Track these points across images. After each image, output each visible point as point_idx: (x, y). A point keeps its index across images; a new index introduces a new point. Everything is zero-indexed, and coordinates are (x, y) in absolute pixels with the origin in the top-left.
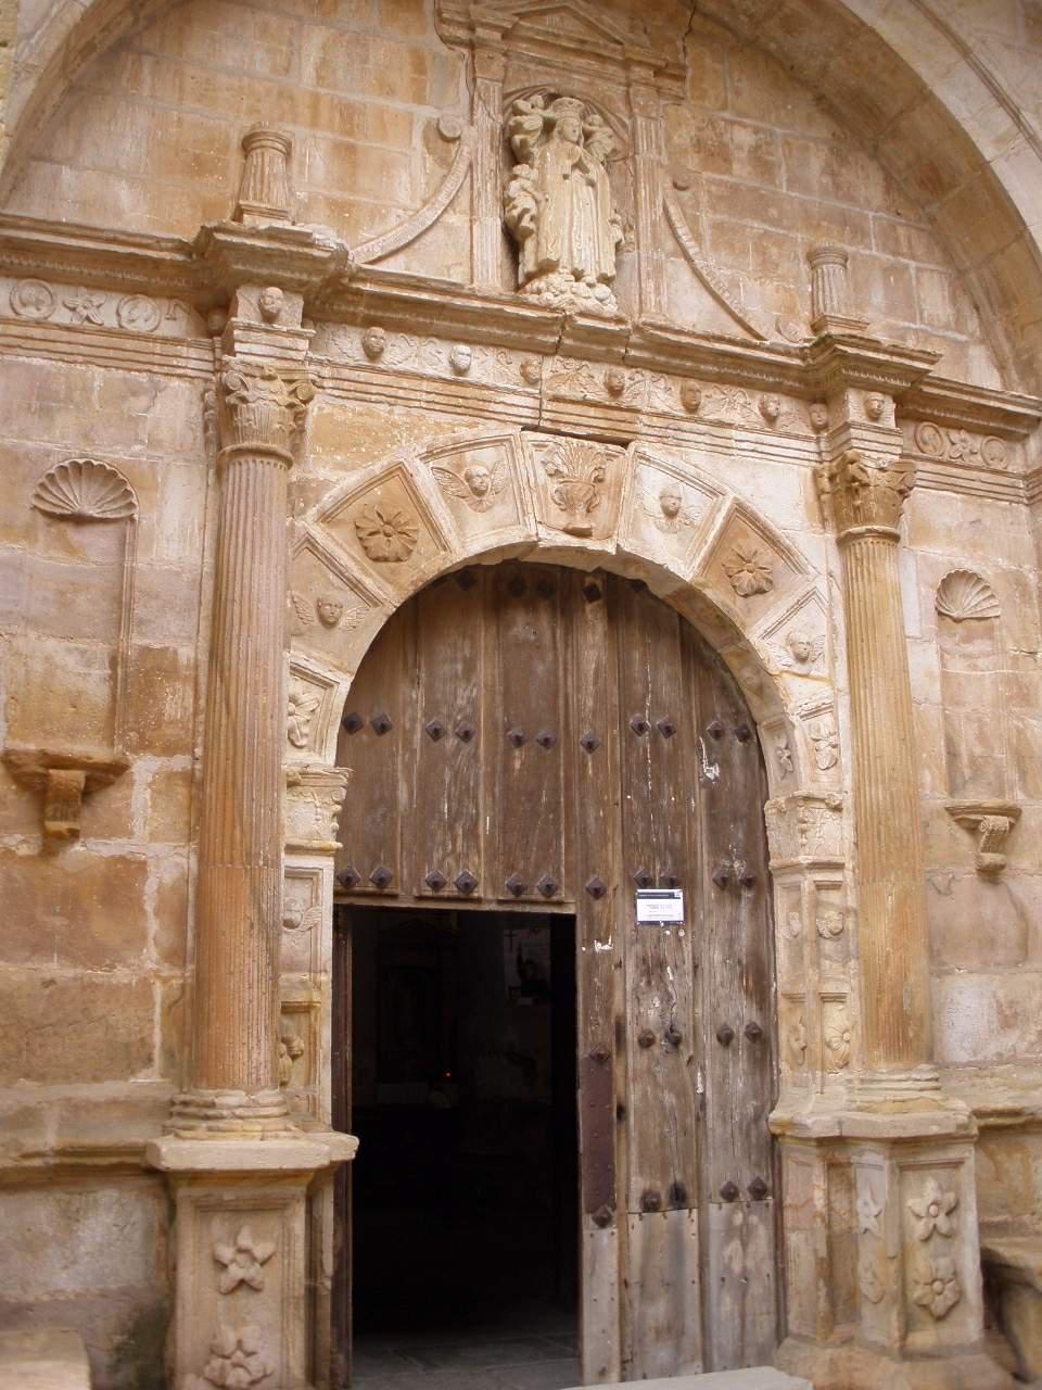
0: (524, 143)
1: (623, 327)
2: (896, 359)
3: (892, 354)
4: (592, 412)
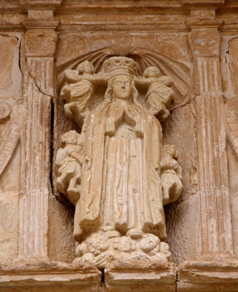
0: (74, 110)
1: (165, 274)
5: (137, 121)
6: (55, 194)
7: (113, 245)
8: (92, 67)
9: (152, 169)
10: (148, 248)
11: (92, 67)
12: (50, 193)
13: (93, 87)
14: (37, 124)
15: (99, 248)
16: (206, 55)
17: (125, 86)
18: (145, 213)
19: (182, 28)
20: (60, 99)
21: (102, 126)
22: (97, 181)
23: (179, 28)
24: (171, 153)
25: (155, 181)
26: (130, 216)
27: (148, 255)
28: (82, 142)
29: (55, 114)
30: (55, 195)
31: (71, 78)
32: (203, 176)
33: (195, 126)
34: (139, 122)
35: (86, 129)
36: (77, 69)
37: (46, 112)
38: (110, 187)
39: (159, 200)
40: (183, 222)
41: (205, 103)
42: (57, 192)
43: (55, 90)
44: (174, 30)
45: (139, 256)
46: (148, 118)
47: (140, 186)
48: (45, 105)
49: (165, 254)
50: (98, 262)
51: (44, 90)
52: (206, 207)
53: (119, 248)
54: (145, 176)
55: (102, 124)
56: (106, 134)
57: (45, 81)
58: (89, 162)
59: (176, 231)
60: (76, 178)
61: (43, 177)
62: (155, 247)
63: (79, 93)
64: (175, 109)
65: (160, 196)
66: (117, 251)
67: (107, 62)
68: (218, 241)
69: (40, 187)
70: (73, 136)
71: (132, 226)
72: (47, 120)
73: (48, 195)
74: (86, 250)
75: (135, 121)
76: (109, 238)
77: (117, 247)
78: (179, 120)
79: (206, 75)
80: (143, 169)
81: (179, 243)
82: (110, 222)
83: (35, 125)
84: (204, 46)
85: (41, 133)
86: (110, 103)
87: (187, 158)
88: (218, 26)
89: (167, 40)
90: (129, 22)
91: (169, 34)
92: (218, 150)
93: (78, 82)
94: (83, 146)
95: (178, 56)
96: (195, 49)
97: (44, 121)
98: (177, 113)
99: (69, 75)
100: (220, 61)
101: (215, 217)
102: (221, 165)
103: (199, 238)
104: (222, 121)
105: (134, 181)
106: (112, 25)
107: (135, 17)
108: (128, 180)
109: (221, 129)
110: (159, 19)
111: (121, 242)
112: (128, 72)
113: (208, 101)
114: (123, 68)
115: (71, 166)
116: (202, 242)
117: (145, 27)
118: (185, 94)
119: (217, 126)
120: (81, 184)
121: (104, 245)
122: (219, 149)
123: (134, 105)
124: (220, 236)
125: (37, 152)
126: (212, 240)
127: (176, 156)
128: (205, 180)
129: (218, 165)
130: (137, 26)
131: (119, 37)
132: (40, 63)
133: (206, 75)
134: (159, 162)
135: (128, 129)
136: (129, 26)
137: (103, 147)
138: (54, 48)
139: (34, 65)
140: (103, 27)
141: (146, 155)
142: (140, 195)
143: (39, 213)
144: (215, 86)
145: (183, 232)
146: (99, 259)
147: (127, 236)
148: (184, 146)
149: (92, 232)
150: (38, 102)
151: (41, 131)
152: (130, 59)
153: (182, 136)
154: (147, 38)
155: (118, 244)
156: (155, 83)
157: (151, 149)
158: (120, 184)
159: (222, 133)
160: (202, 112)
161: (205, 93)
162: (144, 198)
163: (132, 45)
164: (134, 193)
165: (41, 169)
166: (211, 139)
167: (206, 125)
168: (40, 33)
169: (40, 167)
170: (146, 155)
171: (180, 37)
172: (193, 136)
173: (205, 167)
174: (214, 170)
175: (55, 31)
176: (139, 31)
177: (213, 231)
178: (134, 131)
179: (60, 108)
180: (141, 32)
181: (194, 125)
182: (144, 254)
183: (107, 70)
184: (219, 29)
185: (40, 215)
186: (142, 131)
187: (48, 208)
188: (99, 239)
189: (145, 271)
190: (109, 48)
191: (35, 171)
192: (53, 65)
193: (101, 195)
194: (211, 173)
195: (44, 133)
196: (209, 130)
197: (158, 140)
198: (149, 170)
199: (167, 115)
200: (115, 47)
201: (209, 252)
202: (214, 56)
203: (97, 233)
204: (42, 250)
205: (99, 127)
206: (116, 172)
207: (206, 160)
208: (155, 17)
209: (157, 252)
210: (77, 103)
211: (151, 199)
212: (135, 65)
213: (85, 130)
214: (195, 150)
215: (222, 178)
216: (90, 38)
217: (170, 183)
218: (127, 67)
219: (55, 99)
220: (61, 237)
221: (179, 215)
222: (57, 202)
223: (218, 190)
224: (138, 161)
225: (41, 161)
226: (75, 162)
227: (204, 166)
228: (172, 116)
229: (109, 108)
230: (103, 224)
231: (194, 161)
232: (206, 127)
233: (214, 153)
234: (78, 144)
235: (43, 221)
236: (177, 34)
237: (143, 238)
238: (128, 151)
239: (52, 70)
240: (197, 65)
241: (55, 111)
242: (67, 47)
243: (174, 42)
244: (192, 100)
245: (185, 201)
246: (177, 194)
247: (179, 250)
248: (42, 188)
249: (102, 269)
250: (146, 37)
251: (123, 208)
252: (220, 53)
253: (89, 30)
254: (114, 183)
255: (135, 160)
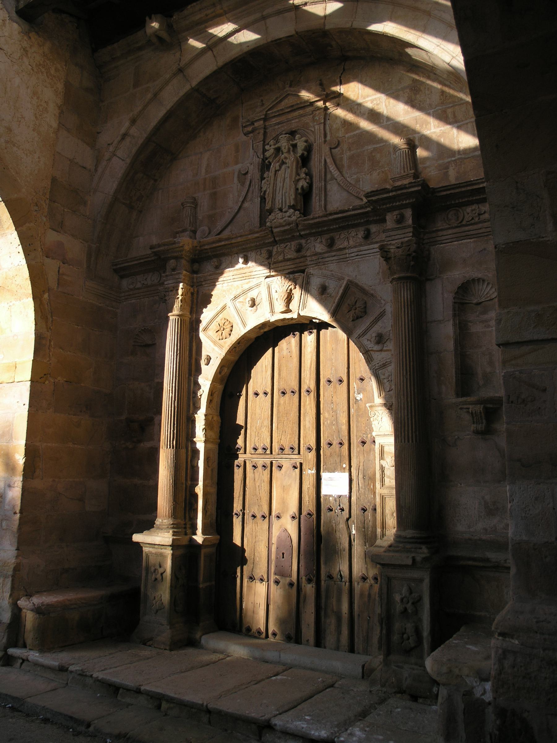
2: (399, 192)
3: (396, 191)
4: (288, 263)
68: (319, 206)
79: (318, 133)
89: (306, 121)
91: (306, 117)
133: (318, 133)
212: (290, 137)
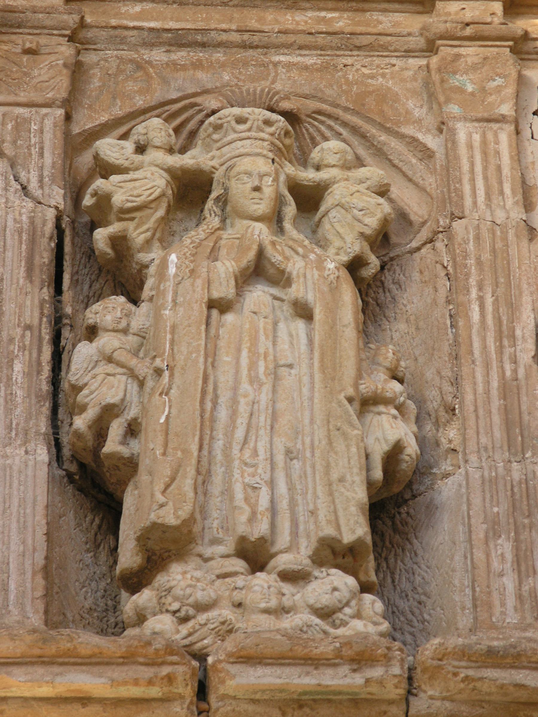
5: (295, 273)
6: (64, 467)
7: (230, 596)
8: (170, 136)
9: (337, 399)
10: (327, 607)
11: (170, 136)
12: (53, 463)
13: (174, 186)
14: (18, 279)
15: (191, 600)
16: (480, 115)
17: (261, 184)
18: (319, 512)
19: (412, 46)
20: (80, 223)
21: (199, 282)
22: (185, 425)
23: (406, 47)
24: (388, 364)
25: (346, 428)
26: (279, 518)
27: (328, 624)
28: (141, 327)
29: (67, 258)
30: (64, 470)
31: (113, 160)
32: (475, 427)
33: (449, 298)
34: (301, 275)
35: (154, 293)
36: (130, 139)
37: (42, 248)
38: (221, 443)
39: (357, 479)
40: (418, 552)
41: (477, 238)
42: (72, 462)
43: (68, 195)
44: (391, 52)
45: (303, 626)
46: (325, 268)
47: (303, 443)
48: (39, 229)
49: (375, 624)
50: (190, 639)
51: (38, 193)
52: (485, 507)
53: (248, 602)
54: (319, 418)
55: (199, 277)
56: (212, 304)
57: (42, 168)
58: (167, 373)
59: (397, 577)
60: (127, 420)
61: (34, 418)
62: (347, 604)
63: (134, 199)
64: (392, 259)
65: (361, 470)
66: (239, 611)
67: (213, 122)
68: (520, 597)
69: (25, 443)
70: (119, 309)
71: (283, 547)
72: (45, 268)
73: (46, 465)
74: (155, 607)
75: (290, 274)
76: (218, 577)
77: (242, 599)
78: (403, 287)
79: (479, 168)
80: (311, 399)
81: (407, 608)
82: (221, 535)
83: (11, 281)
84: (472, 94)
85: (28, 303)
86: (218, 229)
87: (427, 382)
88: (511, 43)
89: (372, 77)
90: (270, 27)
91: (377, 61)
92: (514, 361)
93: (131, 172)
94: (144, 338)
95: (402, 119)
96: (448, 100)
97: (37, 271)
98: (398, 269)
99: (108, 152)
100: (518, 133)
101: (509, 533)
102: (524, 399)
103: (464, 591)
104: (525, 286)
105: (289, 429)
106: (224, 34)
107: (286, 15)
108: (272, 428)
109: (522, 305)
110: (350, 22)
111: (252, 587)
112: (270, 151)
113: (486, 235)
114: (256, 139)
115: (113, 387)
116: (474, 599)
117: (314, 40)
118: (421, 220)
119: (511, 299)
120: (142, 435)
121: (205, 592)
122: (518, 358)
123: (284, 238)
124: (525, 583)
125: (16, 351)
126: (502, 593)
127: (400, 374)
128: (480, 437)
129: (516, 398)
130: (291, 38)
131: (241, 64)
132: (28, 121)
133: (479, 168)
134: (357, 382)
135: (271, 295)
136: (269, 37)
137: (203, 335)
138: (65, 85)
139: (9, 127)
140: (199, 38)
141: (320, 362)
142: (305, 467)
143: (22, 512)
144: (505, 196)
145: (418, 579)
146: (191, 630)
147: (269, 573)
148: (417, 353)
149: (172, 561)
150: (20, 222)
151: (29, 297)
152: (275, 117)
153: (414, 327)
154: (317, 70)
155: (244, 592)
156: (342, 184)
157: (335, 348)
158: (250, 434)
159: (524, 316)
160: (471, 261)
161: (477, 212)
162: (317, 472)
163: (278, 86)
164: (288, 460)
165: (29, 396)
166: (495, 331)
167: (481, 294)
168: (28, 45)
169: (26, 389)
170: (322, 361)
171: (407, 69)
172: (445, 324)
173: (480, 403)
174: (506, 411)
175: (68, 41)
176: (298, 52)
177: (503, 570)
178: (286, 302)
179: (79, 245)
180: (301, 55)
181: (447, 297)
182: (318, 621)
183: (211, 143)
184: (513, 50)
185: (24, 517)
186: (309, 301)
187: (46, 498)
188: (192, 577)
189: (322, 662)
190: (215, 93)
191: (11, 400)
192: (63, 128)
193: (199, 462)
194: (497, 419)
195: (36, 302)
196: (489, 308)
197: (353, 325)
198: (330, 402)
199: (373, 271)
200: (232, 91)
201: (493, 627)
202: (501, 117)
203: (186, 562)
204: (28, 608)
205: (193, 285)
206: (238, 402)
207: (481, 385)
208: (338, 18)
209: (353, 617)
210: (131, 225)
211: (335, 476)
213: (153, 296)
214: (449, 360)
215: (526, 433)
216: (162, 64)
217: (386, 441)
218: (266, 136)
219: (66, 219)
220: (82, 581)
221: (407, 534)
222: (70, 488)
223: (515, 464)
224: (300, 378)
225: (27, 375)
226: (124, 378)
227: (476, 400)
228: (383, 278)
229: (216, 243)
230: (203, 539)
231: (447, 388)
232: (481, 300)
233: (502, 367)
234: (131, 331)
235: (34, 531)
236: (399, 63)
237: (313, 579)
238: (271, 350)
239: (59, 142)
240: (454, 142)
241: (68, 248)
242: (99, 87)
243: (390, 82)
244: (442, 232)
245: (422, 496)
246: (404, 470)
247: (407, 628)
248: (31, 446)
249: (201, 657)
250: (315, 67)
251: (258, 497)
252: (516, 113)
253: (161, 44)
254: (233, 431)
255: (290, 374)
